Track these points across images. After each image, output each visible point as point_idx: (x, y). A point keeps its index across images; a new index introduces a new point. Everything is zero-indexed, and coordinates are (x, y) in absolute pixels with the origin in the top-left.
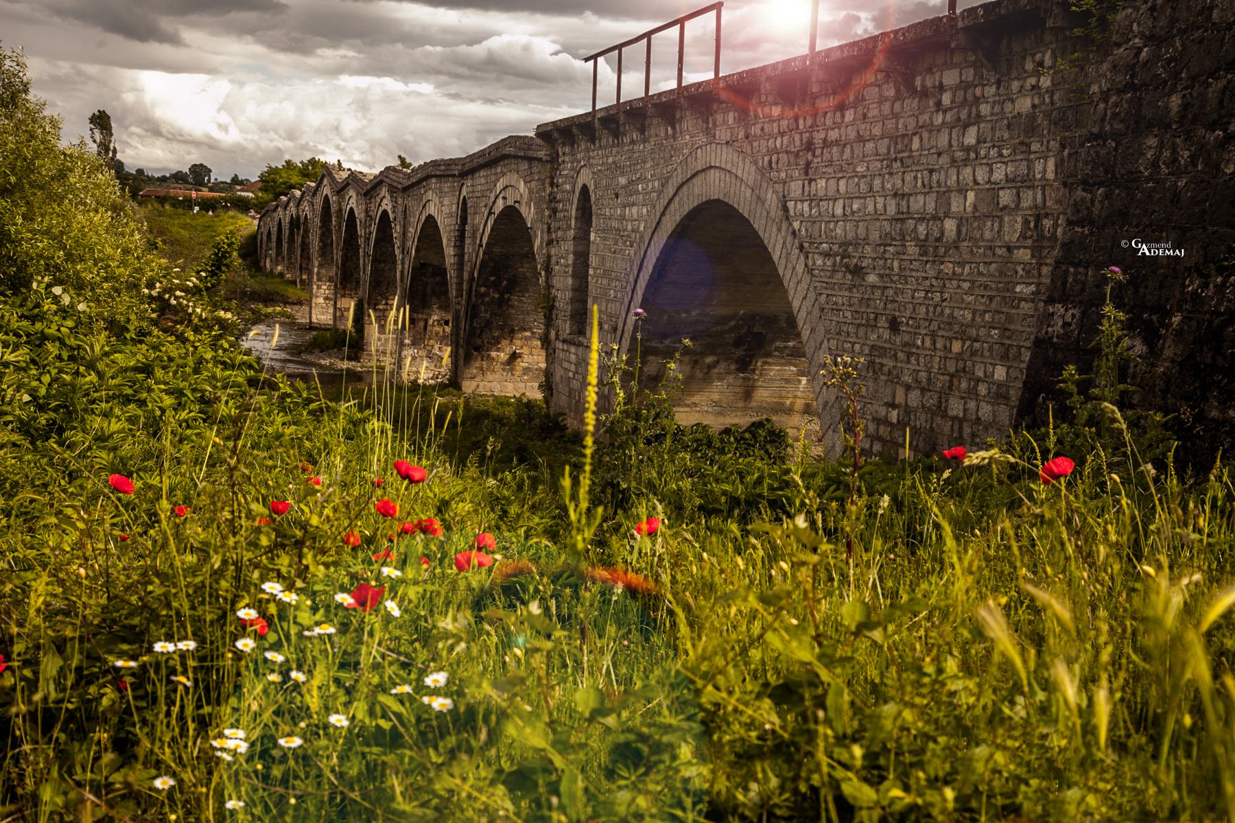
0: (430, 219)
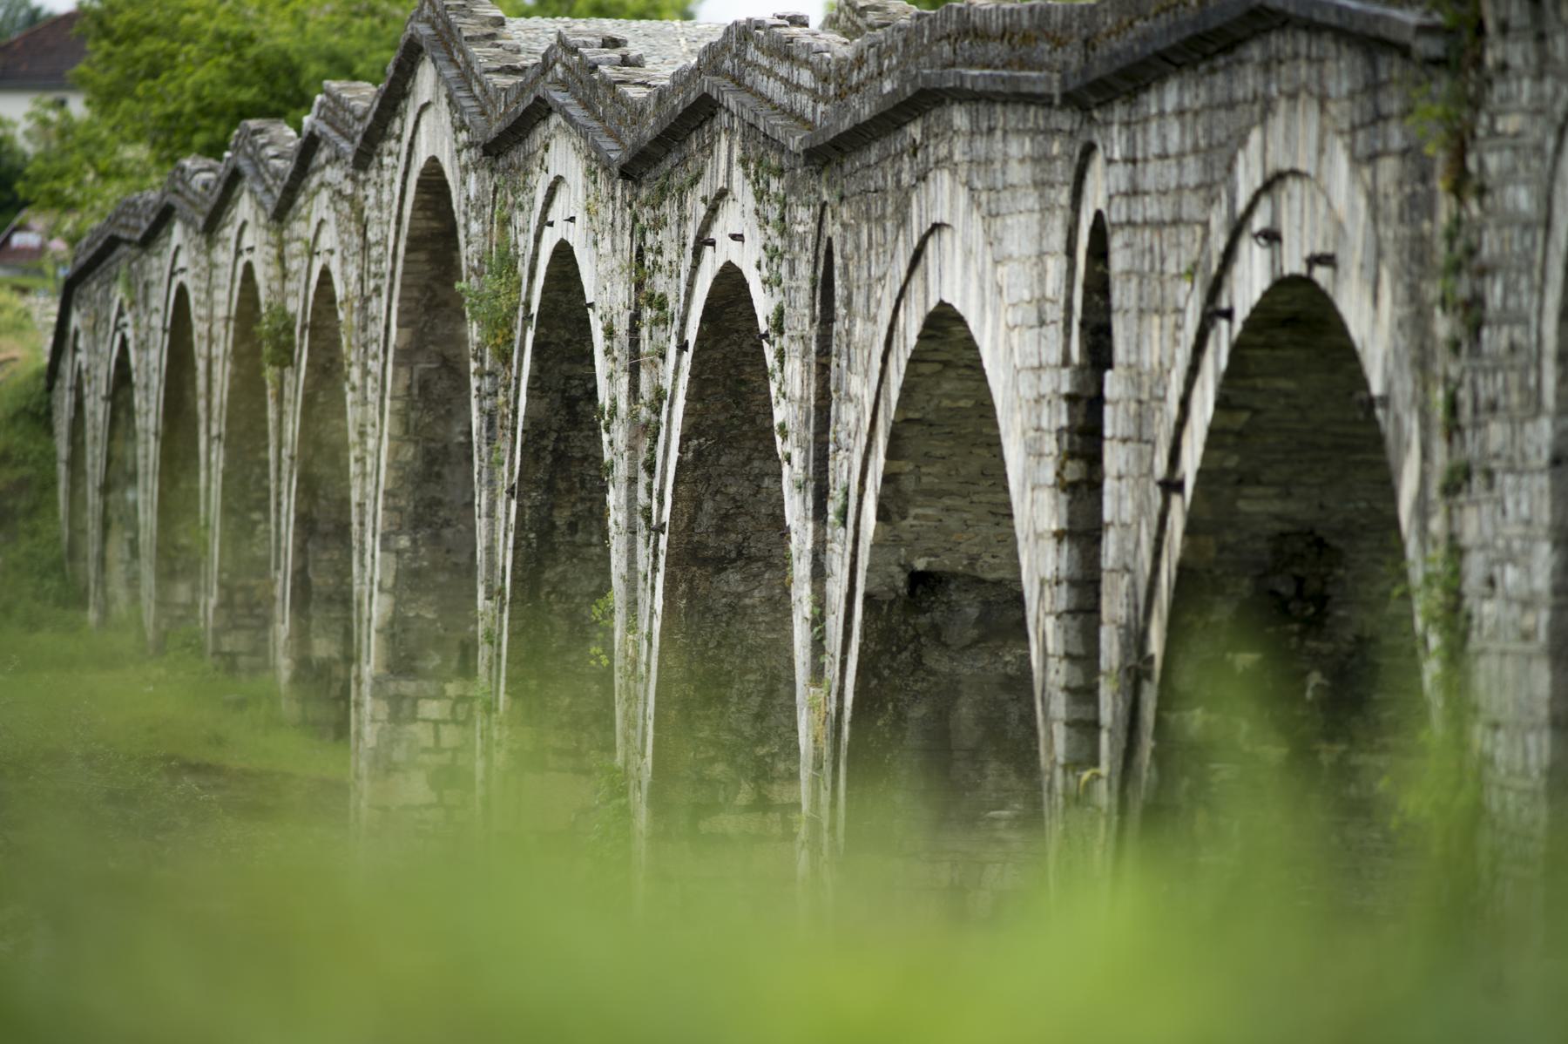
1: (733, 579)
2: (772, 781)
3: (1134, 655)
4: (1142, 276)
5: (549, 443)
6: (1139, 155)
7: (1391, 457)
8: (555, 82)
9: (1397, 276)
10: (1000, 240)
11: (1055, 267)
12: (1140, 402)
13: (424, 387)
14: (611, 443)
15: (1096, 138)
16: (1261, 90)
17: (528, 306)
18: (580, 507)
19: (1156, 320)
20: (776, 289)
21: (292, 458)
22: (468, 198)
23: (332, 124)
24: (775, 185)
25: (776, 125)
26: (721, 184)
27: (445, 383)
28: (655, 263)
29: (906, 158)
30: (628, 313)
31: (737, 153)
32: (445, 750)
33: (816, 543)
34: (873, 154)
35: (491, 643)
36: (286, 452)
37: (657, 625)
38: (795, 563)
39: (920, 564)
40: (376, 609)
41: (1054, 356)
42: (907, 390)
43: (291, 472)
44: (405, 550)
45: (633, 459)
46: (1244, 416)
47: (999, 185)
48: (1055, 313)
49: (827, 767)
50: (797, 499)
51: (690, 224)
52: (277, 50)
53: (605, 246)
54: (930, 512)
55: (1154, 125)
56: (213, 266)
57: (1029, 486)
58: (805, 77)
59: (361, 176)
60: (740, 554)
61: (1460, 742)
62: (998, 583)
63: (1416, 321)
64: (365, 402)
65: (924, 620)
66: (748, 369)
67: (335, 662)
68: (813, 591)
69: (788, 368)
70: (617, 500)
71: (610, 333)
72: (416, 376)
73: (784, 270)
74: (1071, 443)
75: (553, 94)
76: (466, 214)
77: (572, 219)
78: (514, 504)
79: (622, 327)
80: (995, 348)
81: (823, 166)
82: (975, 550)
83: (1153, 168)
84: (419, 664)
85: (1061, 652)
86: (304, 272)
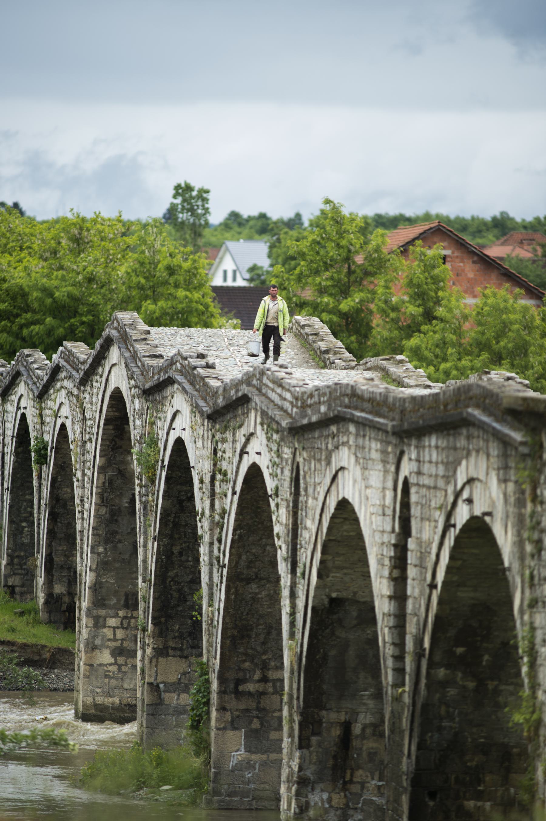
0: (344, 505)
1: (254, 587)
2: (269, 670)
3: (419, 647)
4: (422, 506)
5: (171, 518)
6: (422, 459)
7: (511, 589)
8: (177, 370)
9: (513, 527)
10: (368, 479)
11: (389, 494)
12: (421, 553)
13: (111, 482)
14: (202, 527)
15: (405, 448)
16: (466, 446)
17: (163, 461)
18: (184, 545)
19: (427, 523)
20: (275, 479)
21: (46, 505)
22: (135, 409)
23: (68, 362)
24: (275, 437)
25: (277, 414)
26: (252, 430)
27: (120, 481)
28: (222, 456)
29: (330, 439)
30: (210, 474)
31: (259, 420)
32: (117, 640)
33: (292, 583)
34: (317, 434)
35: (145, 602)
36: (43, 502)
37: (222, 605)
38: (283, 590)
39: (334, 595)
40: (88, 578)
41: (388, 528)
42: (329, 529)
43: (45, 511)
44: (102, 553)
45: (212, 535)
46: (459, 563)
47: (368, 458)
48: (389, 512)
49: (296, 674)
50: (284, 564)
51: (238, 444)
52: (17, 285)
53: (200, 444)
54: (338, 575)
55: (427, 450)
56: (5, 411)
57: (379, 576)
58: (288, 396)
59: (82, 388)
60: (257, 577)
61: (534, 696)
62: (365, 603)
63: (520, 543)
64: (83, 487)
65: (335, 617)
66: (261, 503)
67: (64, 595)
68: (291, 602)
69: (280, 511)
70: (204, 551)
71: (202, 481)
72: (107, 478)
73: (279, 471)
74: (395, 562)
75: (176, 377)
76: (134, 416)
77: (184, 429)
78: (156, 544)
79: (207, 479)
80: (365, 520)
81: (296, 434)
82: (356, 590)
83: (427, 465)
84: (106, 602)
85: (391, 641)
86: (53, 424)
